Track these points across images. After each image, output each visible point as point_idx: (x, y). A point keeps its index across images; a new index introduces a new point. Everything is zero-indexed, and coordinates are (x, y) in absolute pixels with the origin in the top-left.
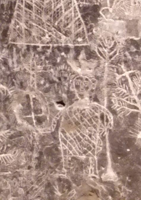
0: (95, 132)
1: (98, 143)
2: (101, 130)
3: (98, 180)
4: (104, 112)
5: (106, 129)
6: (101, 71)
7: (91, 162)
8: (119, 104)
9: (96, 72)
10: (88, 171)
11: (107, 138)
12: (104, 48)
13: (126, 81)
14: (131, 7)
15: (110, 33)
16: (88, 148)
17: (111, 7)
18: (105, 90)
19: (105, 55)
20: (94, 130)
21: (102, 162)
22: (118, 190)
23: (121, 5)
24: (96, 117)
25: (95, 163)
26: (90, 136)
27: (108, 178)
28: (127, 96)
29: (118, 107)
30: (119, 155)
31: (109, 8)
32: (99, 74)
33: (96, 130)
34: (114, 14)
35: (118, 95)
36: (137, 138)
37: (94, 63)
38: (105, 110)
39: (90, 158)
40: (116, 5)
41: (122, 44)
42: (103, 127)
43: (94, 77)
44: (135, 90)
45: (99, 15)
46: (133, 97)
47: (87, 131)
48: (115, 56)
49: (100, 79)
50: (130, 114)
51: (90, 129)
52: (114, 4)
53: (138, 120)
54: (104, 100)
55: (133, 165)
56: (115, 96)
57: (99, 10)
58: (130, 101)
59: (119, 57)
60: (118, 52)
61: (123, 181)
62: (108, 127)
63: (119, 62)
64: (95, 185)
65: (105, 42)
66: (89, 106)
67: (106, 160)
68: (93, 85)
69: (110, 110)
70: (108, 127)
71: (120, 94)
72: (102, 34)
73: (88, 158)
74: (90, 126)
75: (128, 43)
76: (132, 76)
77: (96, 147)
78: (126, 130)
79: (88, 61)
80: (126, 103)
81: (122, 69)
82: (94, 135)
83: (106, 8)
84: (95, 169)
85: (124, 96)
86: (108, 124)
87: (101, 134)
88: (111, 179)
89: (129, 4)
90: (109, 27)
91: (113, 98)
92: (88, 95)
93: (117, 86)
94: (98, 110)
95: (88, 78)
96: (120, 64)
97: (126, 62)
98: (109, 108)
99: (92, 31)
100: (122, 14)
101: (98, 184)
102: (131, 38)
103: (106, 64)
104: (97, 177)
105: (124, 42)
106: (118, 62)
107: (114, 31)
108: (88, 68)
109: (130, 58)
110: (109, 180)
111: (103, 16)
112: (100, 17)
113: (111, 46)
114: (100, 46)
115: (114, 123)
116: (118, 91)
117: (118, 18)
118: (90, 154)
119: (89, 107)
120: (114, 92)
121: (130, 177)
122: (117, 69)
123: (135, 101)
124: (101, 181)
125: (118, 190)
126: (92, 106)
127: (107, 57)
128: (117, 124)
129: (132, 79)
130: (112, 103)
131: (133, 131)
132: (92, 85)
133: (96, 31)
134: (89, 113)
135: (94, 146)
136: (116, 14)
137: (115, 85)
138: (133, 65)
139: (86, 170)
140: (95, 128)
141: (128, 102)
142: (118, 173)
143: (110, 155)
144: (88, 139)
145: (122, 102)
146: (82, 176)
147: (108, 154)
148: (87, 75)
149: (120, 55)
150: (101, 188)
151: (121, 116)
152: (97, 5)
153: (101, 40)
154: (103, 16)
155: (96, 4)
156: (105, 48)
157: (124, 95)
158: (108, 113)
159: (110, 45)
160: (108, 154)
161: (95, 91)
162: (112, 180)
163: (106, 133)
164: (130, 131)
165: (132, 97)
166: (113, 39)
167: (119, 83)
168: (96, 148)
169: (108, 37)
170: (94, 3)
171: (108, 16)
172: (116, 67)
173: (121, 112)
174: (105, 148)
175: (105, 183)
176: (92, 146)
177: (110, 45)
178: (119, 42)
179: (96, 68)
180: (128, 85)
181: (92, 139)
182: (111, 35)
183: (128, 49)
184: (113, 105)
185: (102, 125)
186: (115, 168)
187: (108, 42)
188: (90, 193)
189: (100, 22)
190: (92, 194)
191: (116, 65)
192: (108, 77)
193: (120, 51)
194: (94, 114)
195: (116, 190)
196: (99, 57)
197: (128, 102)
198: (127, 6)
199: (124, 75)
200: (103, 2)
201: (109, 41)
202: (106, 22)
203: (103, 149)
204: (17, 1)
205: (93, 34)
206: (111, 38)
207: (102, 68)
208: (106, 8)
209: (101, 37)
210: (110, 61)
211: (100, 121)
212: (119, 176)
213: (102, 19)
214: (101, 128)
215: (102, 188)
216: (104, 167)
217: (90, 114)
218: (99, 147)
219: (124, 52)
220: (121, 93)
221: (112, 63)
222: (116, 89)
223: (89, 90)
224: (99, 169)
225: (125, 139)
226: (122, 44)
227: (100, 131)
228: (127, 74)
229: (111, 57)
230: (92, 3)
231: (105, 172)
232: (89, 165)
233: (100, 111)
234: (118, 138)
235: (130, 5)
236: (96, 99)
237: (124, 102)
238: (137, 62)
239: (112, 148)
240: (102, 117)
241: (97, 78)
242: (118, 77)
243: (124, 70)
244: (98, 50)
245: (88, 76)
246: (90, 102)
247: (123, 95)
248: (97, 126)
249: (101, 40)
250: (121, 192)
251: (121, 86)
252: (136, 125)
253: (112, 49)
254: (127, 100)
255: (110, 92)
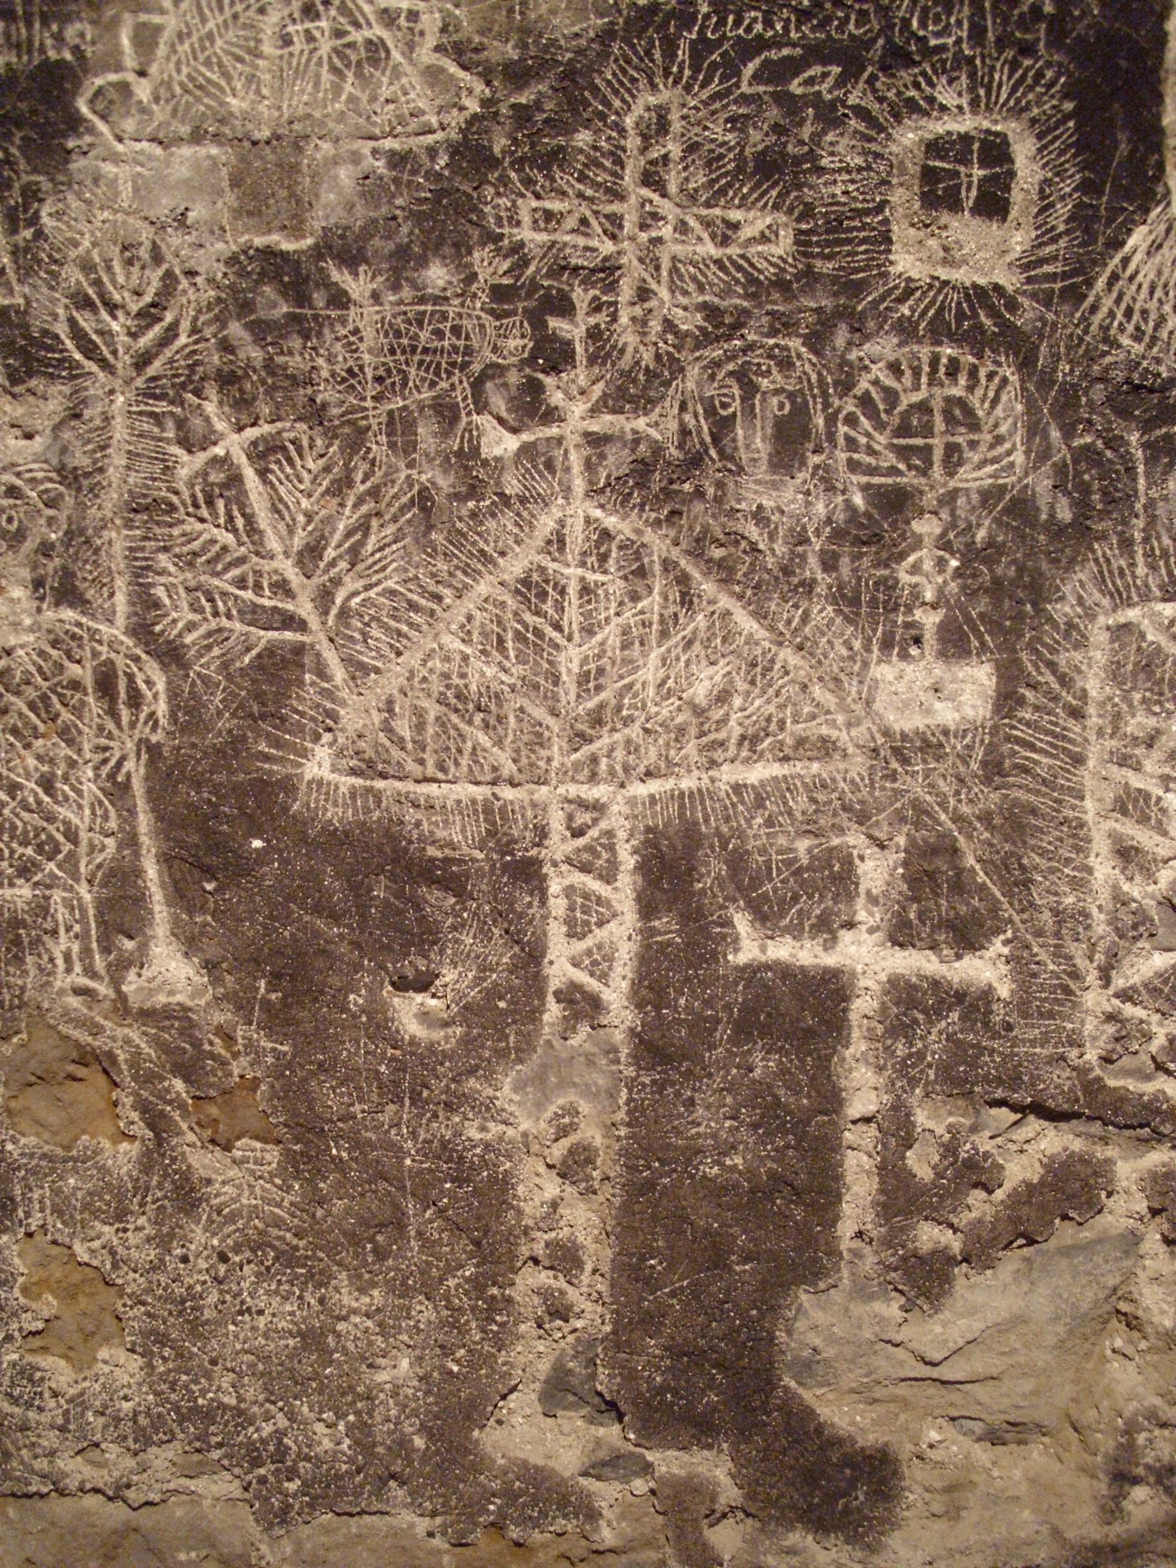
0: (72, 764)
1: (93, 821)
2: (106, 749)
3: (107, 1005)
4: (113, 655)
5: (130, 745)
6: (89, 441)
7: (62, 914)
8: (196, 608)
9: (64, 450)
10: (52, 960)
11: (138, 787)
12: (104, 315)
13: (235, 479)
14: (260, 62)
15: (139, 224)
16: (40, 849)
17: (142, 74)
18: (117, 542)
19: (114, 353)
20: (64, 751)
21: (121, 912)
22: (219, 1048)
23: (201, 58)
24: (76, 685)
25: (83, 920)
26: (47, 784)
27: (159, 989)
28: (242, 561)
29: (191, 627)
30: (209, 872)
31: (131, 77)
32: (79, 459)
33: (79, 751)
34: (160, 113)
35: (189, 561)
36: (300, 777)
37: (55, 399)
38: (123, 649)
39: (57, 895)
40: (174, 59)
41: (211, 281)
42: (116, 732)
43: (53, 475)
44: (282, 527)
45: (75, 123)
46: (275, 564)
47: (31, 762)
48: (168, 353)
49: (85, 483)
50: (259, 656)
51: (41, 751)
52: (162, 50)
53: (301, 683)
54: (112, 595)
55: (287, 920)
56: (172, 569)
57: (74, 94)
58: (258, 588)
59: (194, 352)
60: (185, 325)
61: (242, 1004)
62: (145, 731)
63: (190, 382)
64: (96, 1030)
65: (114, 281)
66: (31, 630)
67: (140, 900)
68: (51, 521)
69: (147, 644)
70: (145, 731)
71: (195, 554)
72: (92, 234)
73: (47, 898)
74: (43, 736)
75: (243, 274)
76: (264, 453)
77: (84, 836)
78: (237, 742)
79: (17, 389)
80: (236, 597)
81: (207, 420)
82: (66, 779)
83: (113, 77)
84: (86, 952)
85: (219, 567)
86: (142, 717)
87: (105, 771)
88: (171, 993)
89: (249, 51)
90: (136, 190)
91: (162, 580)
92: (26, 574)
93: (181, 514)
94: (80, 646)
95: (18, 482)
96: (198, 393)
97: (227, 380)
98: (142, 631)
99: (34, 220)
100: (208, 106)
101: (108, 1024)
102: (259, 241)
103: (115, 402)
104: (103, 989)
105: (220, 270)
106: (183, 386)
107: (163, 207)
108: (18, 432)
109: (256, 354)
110: (162, 999)
111: (101, 126)
112: (79, 136)
113: (148, 299)
114: (86, 303)
115: (173, 716)
116: (190, 538)
117: (185, 130)
118: (52, 875)
119: (31, 638)
120: (166, 549)
121: (275, 978)
122: (181, 424)
123: (282, 587)
124: (121, 1007)
125: (219, 1048)
126: (49, 631)
127: (123, 362)
128: (188, 711)
129: (263, 473)
130: (157, 605)
131: (277, 743)
132: (42, 521)
133: (57, 215)
134: (33, 669)
135: (72, 835)
136: (175, 111)
137: (172, 508)
138: (270, 391)
139: (39, 956)
140: (70, 742)
141: (248, 595)
142: (210, 966)
143: (160, 873)
144: (39, 802)
145: (211, 600)
146: (23, 989)
147: (151, 870)
148: (13, 465)
149: (196, 342)
150: (128, 1041)
151: (211, 672)
152: (61, 63)
153: (87, 266)
154: (101, 126)
155: (52, 55)
156: (112, 308)
157: (219, 559)
158: (137, 659)
159: (138, 294)
160: (151, 870)
161: (60, 548)
162: (179, 998)
163: (129, 765)
164: (263, 747)
165: (266, 566)
166: (157, 257)
167: (193, 497)
168: (83, 848)
169: (125, 248)
170: (42, 50)
171: (129, 125)
172: (178, 410)
173: (209, 648)
174: (131, 841)
175: (147, 1015)
176: (60, 838)
177: (138, 294)
178: (191, 273)
179: (57, 428)
180: (242, 508)
181: (57, 802)
182: (146, 234)
183: (246, 307)
184: (166, 615)
185: (110, 725)
186: (190, 943)
187: (128, 276)
188: (72, 1068)
189: (78, 164)
190: (81, 1072)
191: (172, 403)
192: (128, 468)
193: (195, 319)
194: (60, 668)
195: (207, 1047)
196: (79, 366)
197: (248, 595)
198: (240, 60)
199: (219, 451)
200: (99, 46)
201: (135, 270)
202: (116, 159)
203: (120, 847)
204: (1158, 1157)
205: (39, 234)
206: (144, 253)
207: (98, 422)
208: (113, 77)
209: (88, 252)
210: (140, 382)
211: (94, 705)
212: (216, 981)
213: (91, 145)
214: (103, 741)
215: (127, 1040)
216: (131, 938)
217: (40, 670)
218: (97, 838)
219: (224, 326)
220: (204, 549)
221: (149, 394)
222: (176, 532)
223: (29, 545)
224: (106, 950)
225: (235, 787)
226: (211, 281)
227: (99, 757)
228: (233, 445)
229: (142, 361)
230: (29, 52)
231: (139, 960)
232: (54, 933)
233: (95, 654)
234: (198, 785)
235: (259, 56)
236: (68, 592)
237: (224, 594)
238: (293, 377)
239: (167, 839)
240: (106, 683)
241: (70, 477)
242: (188, 464)
243: (220, 426)
244: (72, 321)
245: (18, 475)
246: (39, 610)
247: (217, 558)
248: (80, 733)
249: (87, 266)
250: (236, 1055)
251: (204, 512)
252: (297, 712)
253: (148, 316)
254: (241, 583)
255: (143, 549)
